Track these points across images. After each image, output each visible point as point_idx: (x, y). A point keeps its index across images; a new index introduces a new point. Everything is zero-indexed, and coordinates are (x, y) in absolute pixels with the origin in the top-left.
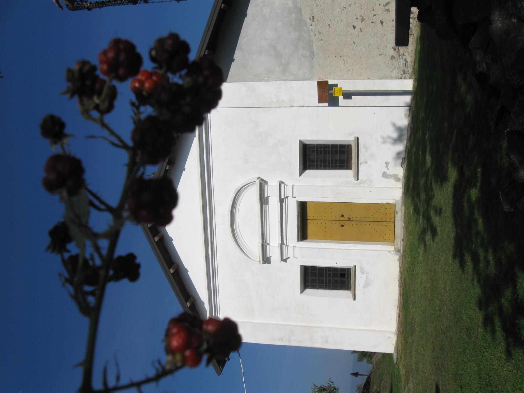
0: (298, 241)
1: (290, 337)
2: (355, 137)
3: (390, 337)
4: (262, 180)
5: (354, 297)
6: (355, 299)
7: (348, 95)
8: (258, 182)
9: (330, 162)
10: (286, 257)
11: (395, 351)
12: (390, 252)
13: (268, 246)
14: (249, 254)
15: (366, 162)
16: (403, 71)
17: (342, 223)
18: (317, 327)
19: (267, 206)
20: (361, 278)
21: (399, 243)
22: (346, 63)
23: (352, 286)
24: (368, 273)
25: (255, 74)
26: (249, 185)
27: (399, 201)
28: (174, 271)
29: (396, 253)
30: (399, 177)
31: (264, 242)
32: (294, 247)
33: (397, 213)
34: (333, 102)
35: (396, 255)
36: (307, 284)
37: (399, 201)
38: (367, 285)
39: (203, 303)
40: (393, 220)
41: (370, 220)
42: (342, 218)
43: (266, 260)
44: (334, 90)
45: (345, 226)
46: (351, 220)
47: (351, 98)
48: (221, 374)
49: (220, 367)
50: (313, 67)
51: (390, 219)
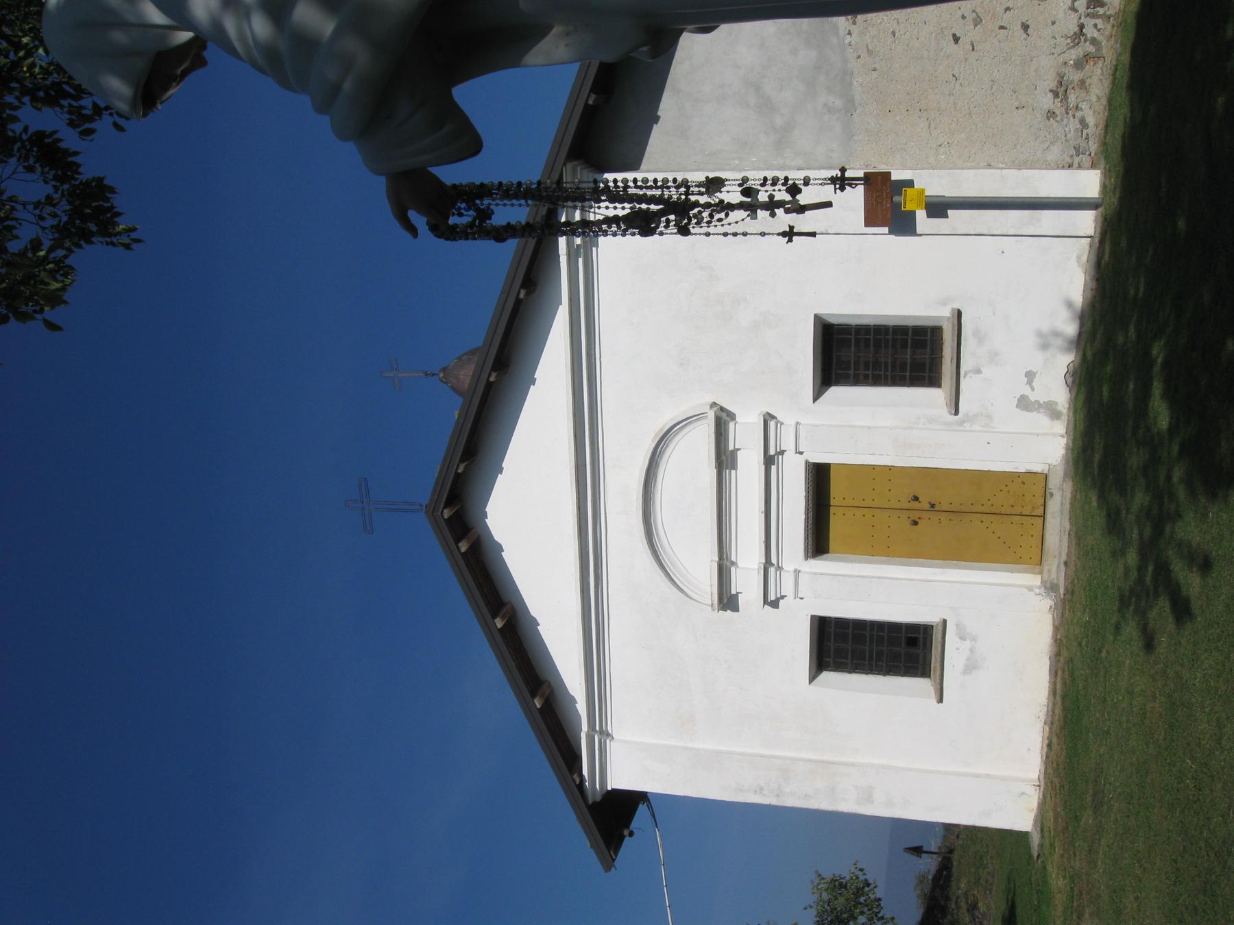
0: (807, 557)
2: (953, 309)
3: (1023, 793)
4: (722, 409)
6: (940, 700)
7: (938, 208)
12: (1030, 589)
13: (733, 569)
15: (978, 371)
16: (1075, 148)
17: (915, 516)
19: (733, 472)
22: (933, 126)
30: (1060, 408)
32: (797, 572)
33: (1052, 495)
34: (902, 224)
38: (971, 667)
40: (1040, 511)
42: (915, 505)
43: (727, 601)
44: (905, 196)
45: (920, 522)
46: (937, 508)
49: (612, 852)
50: (853, 136)
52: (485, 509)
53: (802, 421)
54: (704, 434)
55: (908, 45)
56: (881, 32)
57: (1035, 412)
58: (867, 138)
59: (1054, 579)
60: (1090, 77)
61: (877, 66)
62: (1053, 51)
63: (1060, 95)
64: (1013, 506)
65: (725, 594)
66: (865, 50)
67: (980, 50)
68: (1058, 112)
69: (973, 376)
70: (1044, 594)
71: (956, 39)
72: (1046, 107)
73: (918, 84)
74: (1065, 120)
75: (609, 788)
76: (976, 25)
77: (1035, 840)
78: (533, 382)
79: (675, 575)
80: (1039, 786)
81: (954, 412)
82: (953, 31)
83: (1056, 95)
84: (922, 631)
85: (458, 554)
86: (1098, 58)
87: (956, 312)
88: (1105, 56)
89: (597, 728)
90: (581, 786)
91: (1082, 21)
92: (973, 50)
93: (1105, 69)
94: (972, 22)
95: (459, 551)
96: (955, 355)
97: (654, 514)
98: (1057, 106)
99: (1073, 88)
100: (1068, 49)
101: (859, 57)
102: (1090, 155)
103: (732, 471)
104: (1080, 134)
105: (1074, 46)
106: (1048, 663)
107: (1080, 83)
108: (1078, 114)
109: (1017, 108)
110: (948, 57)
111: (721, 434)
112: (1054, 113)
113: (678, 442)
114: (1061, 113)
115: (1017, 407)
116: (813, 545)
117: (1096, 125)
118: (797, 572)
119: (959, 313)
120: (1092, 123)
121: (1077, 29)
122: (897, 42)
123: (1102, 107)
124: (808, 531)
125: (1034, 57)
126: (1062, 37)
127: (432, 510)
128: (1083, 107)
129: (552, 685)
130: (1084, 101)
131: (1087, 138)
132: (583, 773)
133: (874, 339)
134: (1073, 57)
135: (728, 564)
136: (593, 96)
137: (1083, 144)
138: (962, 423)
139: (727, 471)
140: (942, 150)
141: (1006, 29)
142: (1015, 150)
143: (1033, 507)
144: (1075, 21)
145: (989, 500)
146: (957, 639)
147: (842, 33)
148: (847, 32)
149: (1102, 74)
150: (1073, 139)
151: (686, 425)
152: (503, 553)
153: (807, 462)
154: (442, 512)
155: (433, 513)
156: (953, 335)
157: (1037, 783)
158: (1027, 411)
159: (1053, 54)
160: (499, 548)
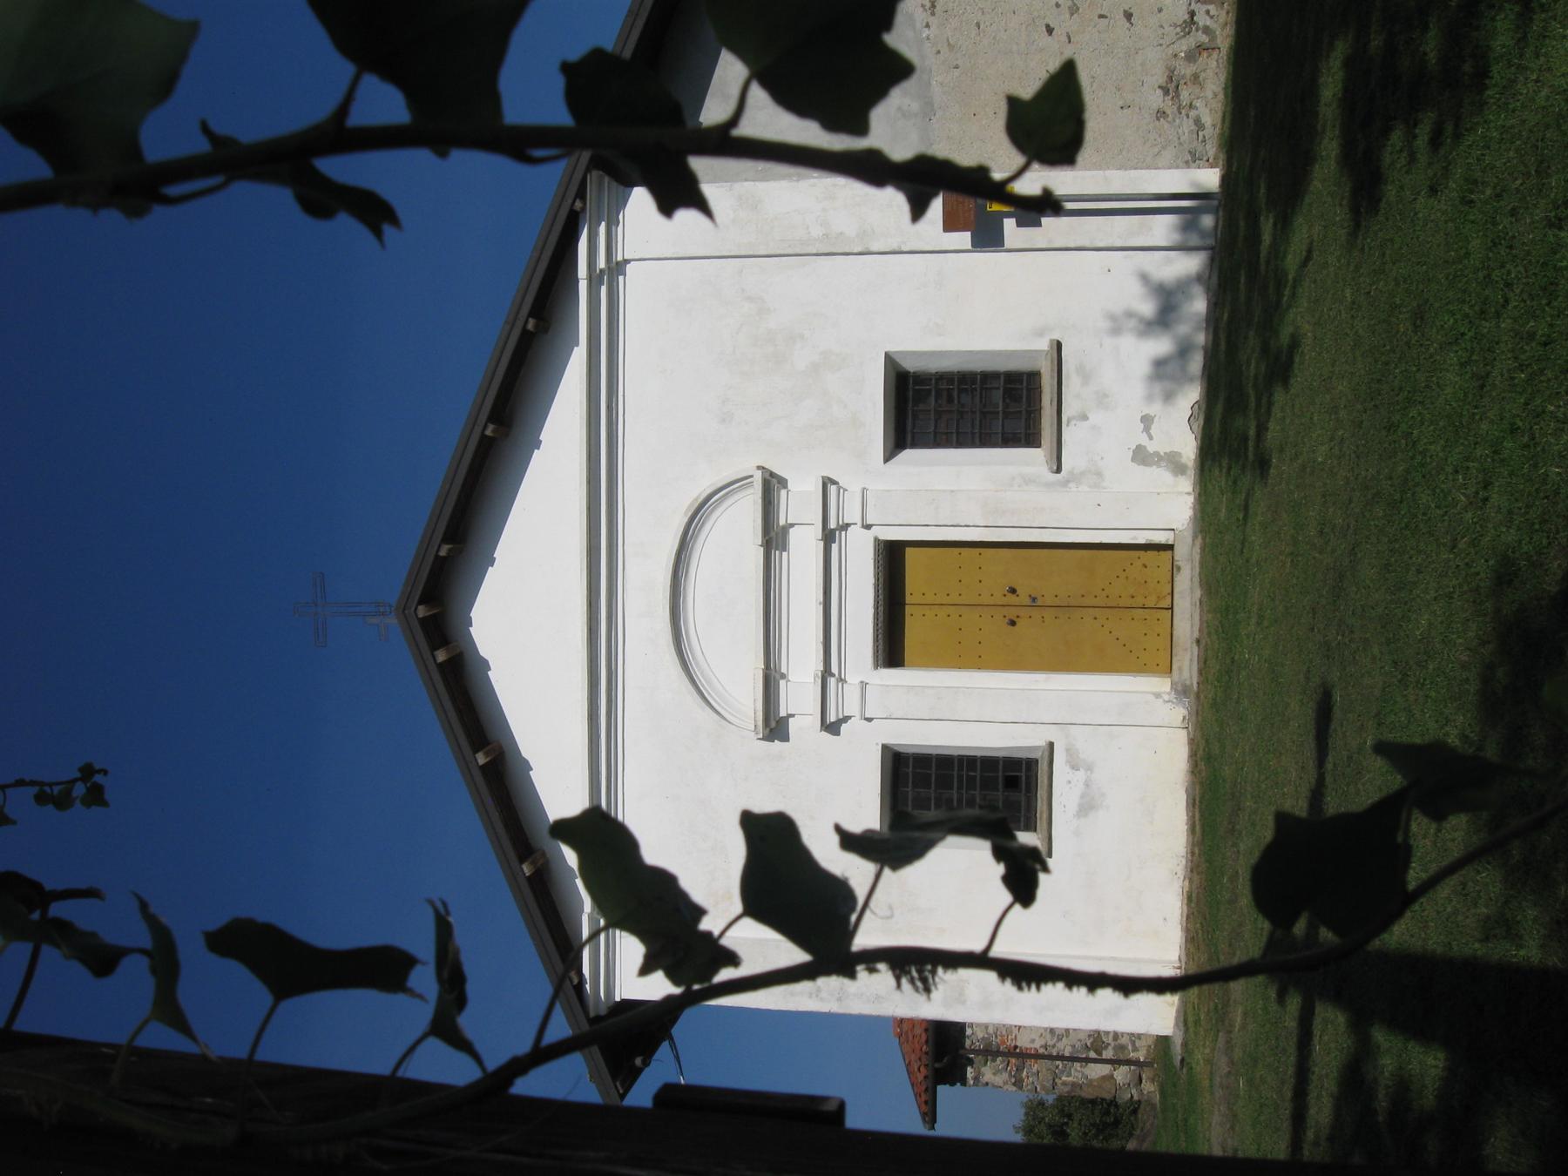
0: (876, 666)
2: (1052, 341)
4: (772, 474)
8: (758, 475)
11: (1177, 1025)
12: (1158, 695)
13: (782, 683)
15: (1084, 417)
19: (784, 554)
21: (1187, 663)
29: (1176, 698)
30: (1184, 460)
32: (864, 685)
33: (1179, 568)
38: (1087, 807)
40: (1167, 603)
42: (1012, 599)
43: (775, 727)
45: (1020, 623)
49: (618, 1084)
50: (932, 144)
54: (748, 505)
55: (994, 38)
56: (964, 23)
57: (1155, 467)
59: (1185, 680)
60: (1204, 70)
61: (960, 62)
62: (1161, 42)
63: (1171, 91)
64: (1133, 597)
65: (772, 701)
66: (946, 44)
67: (1077, 42)
68: (1169, 112)
69: (1078, 423)
70: (1175, 700)
71: (1050, 30)
72: (1155, 106)
73: (1006, 82)
74: (1177, 121)
75: (618, 999)
76: (1072, 14)
77: (1178, 1041)
78: (538, 444)
79: (709, 694)
81: (1055, 468)
82: (1047, 20)
83: (1166, 91)
84: (1024, 766)
85: (434, 665)
86: (1213, 49)
87: (1055, 343)
88: (1220, 46)
90: (579, 988)
91: (1192, 7)
92: (1070, 42)
93: (1221, 61)
94: (1067, 11)
95: (435, 660)
96: (1056, 395)
98: (1168, 106)
99: (1185, 83)
100: (1178, 39)
101: (939, 52)
102: (1208, 161)
103: (784, 553)
104: (1195, 136)
105: (1185, 36)
106: (1184, 797)
107: (1192, 78)
108: (1193, 113)
109: (1122, 108)
110: (1042, 50)
111: (770, 502)
112: (1164, 113)
114: (1172, 113)
115: (1132, 461)
116: (884, 651)
117: (1213, 125)
118: (864, 685)
119: (1059, 346)
120: (1208, 123)
121: (1186, 17)
122: (981, 35)
123: (1220, 105)
124: (877, 630)
125: (1139, 49)
126: (1171, 26)
127: (403, 610)
128: (1198, 105)
129: (548, 856)
130: (1198, 98)
132: (584, 972)
133: (967, 776)
134: (1184, 48)
135: (778, 676)
136: (491, 427)
137: (1200, 148)
138: (1066, 483)
141: (1106, 17)
142: (1121, 156)
143: (1159, 597)
144: (1185, 8)
145: (1103, 590)
146: (1068, 769)
147: (918, 25)
148: (924, 24)
149: (1218, 67)
150: (1187, 142)
151: (727, 493)
152: (489, 673)
153: (876, 539)
154: (416, 609)
155: (404, 609)
156: (1052, 370)
157: (1178, 965)
158: (1146, 465)
159: (1161, 45)
160: (485, 665)
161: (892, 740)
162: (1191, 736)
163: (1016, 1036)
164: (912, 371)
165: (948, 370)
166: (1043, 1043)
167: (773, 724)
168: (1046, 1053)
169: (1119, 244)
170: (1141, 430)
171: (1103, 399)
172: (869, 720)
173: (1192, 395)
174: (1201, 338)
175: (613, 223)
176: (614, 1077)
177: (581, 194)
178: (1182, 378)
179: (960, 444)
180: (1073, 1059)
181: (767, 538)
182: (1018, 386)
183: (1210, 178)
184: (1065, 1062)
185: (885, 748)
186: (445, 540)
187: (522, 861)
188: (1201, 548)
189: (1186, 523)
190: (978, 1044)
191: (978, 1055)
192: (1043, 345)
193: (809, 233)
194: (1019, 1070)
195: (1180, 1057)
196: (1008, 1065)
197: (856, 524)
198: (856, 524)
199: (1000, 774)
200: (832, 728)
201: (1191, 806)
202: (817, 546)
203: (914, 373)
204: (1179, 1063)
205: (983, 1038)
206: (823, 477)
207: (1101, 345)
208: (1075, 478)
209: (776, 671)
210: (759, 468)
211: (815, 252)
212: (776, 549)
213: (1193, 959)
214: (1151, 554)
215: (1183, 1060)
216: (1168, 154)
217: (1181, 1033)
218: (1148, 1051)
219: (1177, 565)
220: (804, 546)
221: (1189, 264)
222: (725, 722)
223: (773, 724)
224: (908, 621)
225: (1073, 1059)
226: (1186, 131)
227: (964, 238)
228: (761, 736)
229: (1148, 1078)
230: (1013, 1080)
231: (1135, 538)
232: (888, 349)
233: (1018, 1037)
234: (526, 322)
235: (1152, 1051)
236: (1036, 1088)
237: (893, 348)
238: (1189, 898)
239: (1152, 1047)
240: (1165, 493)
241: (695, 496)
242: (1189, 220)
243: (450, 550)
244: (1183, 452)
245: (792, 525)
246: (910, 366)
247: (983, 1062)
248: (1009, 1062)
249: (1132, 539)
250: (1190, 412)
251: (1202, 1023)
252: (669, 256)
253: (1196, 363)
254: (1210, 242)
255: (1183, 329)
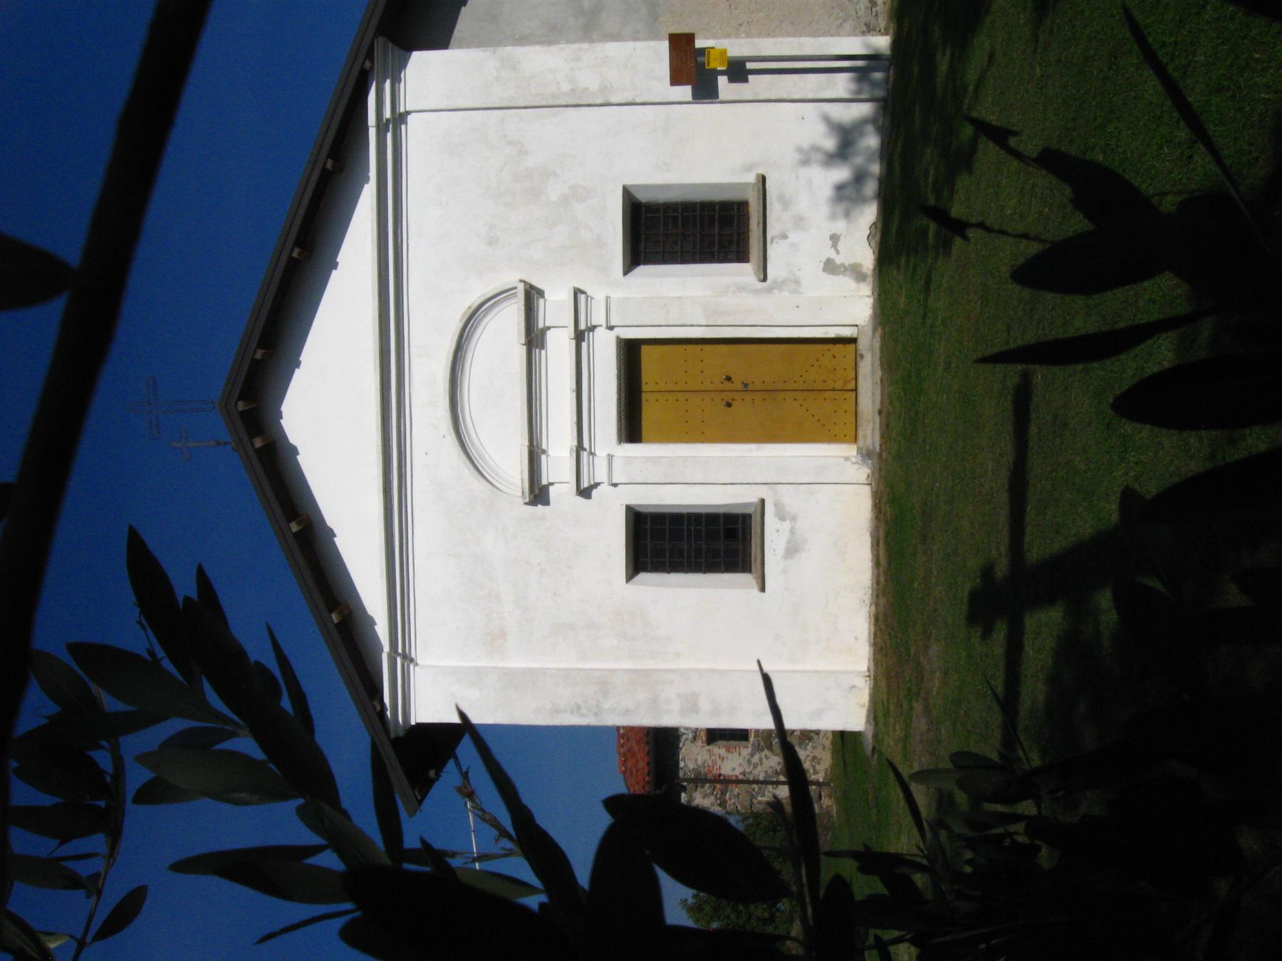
0: (620, 441)
1: (598, 701)
2: (758, 175)
3: (854, 687)
4: (532, 287)
5: (760, 581)
6: (763, 589)
7: (738, 71)
8: (521, 287)
9: (698, 247)
10: (589, 481)
11: (868, 721)
12: (847, 459)
13: (543, 457)
14: (496, 480)
15: (785, 237)
16: (866, 24)
17: (728, 397)
18: (668, 671)
19: (543, 352)
20: (778, 531)
21: (870, 432)
22: (733, 7)
23: (756, 556)
24: (794, 519)
25: (517, 37)
26: (498, 298)
27: (867, 328)
28: (300, 530)
29: (862, 460)
30: (865, 270)
31: (533, 446)
32: (610, 457)
33: (862, 356)
34: (705, 90)
35: (862, 465)
36: (642, 560)
37: (867, 328)
38: (793, 550)
39: (372, 622)
40: (852, 386)
41: (794, 386)
42: (728, 385)
43: (538, 494)
44: (709, 55)
45: (735, 404)
46: (750, 387)
47: (746, 81)
48: (418, 811)
49: (416, 792)
50: (657, 18)
51: (846, 382)
52: (280, 407)
53: (612, 295)
58: (671, 20)
65: (536, 482)
75: (413, 723)
77: (869, 735)
80: (869, 676)
81: (762, 277)
84: (740, 521)
89: (400, 651)
97: (461, 391)
111: (531, 310)
113: (486, 325)
118: (610, 457)
124: (620, 412)
131: (876, 15)
137: (874, 22)
138: (770, 290)
139: (537, 350)
140: (742, 29)
146: (776, 520)
151: (495, 303)
154: (236, 403)
160: (294, 451)
161: (633, 501)
162: (875, 490)
163: (720, 767)
164: (644, 201)
165: (673, 200)
166: (742, 770)
167: (537, 491)
168: (744, 779)
169: (810, 96)
170: (830, 246)
171: (799, 222)
172: (615, 485)
173: (869, 214)
174: (876, 168)
175: (396, 80)
176: (413, 787)
177: (370, 55)
178: (860, 200)
179: (684, 261)
180: (765, 782)
181: (529, 338)
182: (732, 213)
183: (882, 43)
184: (760, 785)
185: (629, 509)
186: (259, 346)
187: (331, 611)
188: (881, 338)
189: (867, 319)
190: (689, 774)
191: (690, 783)
192: (751, 178)
193: (560, 88)
194: (723, 793)
195: (871, 747)
196: (714, 789)
197: (601, 326)
198: (601, 326)
199: (722, 526)
200: (585, 493)
201: (875, 546)
202: (570, 343)
203: (646, 203)
204: (870, 751)
205: (694, 769)
206: (574, 288)
207: (797, 179)
208: (779, 285)
209: (538, 447)
210: (521, 281)
211: (564, 103)
212: (537, 347)
213: (882, 665)
214: (839, 346)
215: (874, 748)
216: (848, 26)
217: (872, 727)
218: (826, 773)
219: (860, 352)
220: (559, 345)
221: (863, 110)
222: (496, 490)
223: (537, 491)
224: (644, 404)
225: (765, 782)
226: (863, 7)
227: (685, 92)
228: (527, 500)
229: (826, 795)
230: (719, 802)
231: (826, 333)
232: (625, 183)
233: (722, 767)
234: (325, 163)
235: (829, 773)
236: (737, 807)
237: (630, 181)
238: (877, 619)
239: (829, 770)
240: (851, 296)
241: (469, 305)
242: (861, 75)
243: (263, 354)
244: (863, 263)
245: (549, 328)
246: (642, 197)
247: (694, 789)
248: (715, 787)
249: (824, 334)
250: (869, 232)
251: (891, 713)
252: (443, 107)
253: (871, 187)
254: (880, 93)
255: (859, 160)
